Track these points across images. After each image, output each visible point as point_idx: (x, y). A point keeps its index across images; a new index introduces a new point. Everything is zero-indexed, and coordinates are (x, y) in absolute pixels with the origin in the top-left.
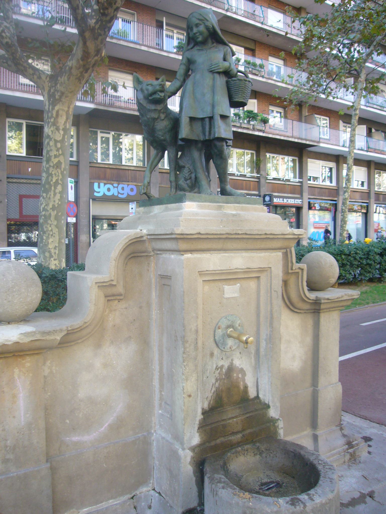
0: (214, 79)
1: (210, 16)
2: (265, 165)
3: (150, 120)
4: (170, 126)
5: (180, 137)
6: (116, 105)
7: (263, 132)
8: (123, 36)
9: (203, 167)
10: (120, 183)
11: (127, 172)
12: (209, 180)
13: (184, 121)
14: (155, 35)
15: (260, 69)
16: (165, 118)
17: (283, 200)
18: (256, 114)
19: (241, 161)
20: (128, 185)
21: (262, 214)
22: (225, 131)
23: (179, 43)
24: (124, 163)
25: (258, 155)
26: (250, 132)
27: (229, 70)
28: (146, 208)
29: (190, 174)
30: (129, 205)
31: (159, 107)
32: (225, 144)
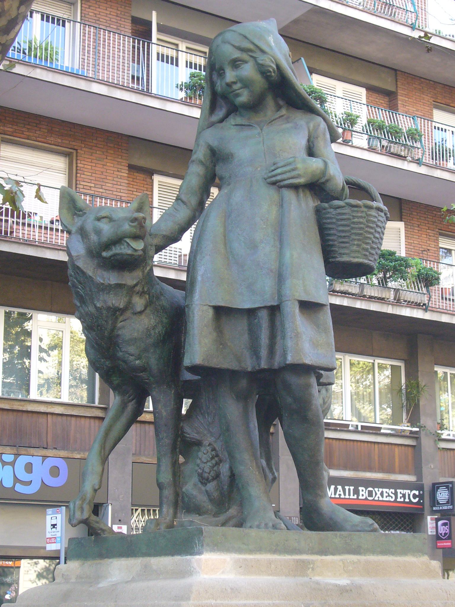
0: (281, 205)
1: (271, 40)
2: (433, 398)
3: (104, 312)
4: (160, 329)
5: (187, 362)
6: (17, 238)
7: (425, 308)
8: (45, 57)
9: (252, 445)
10: (22, 451)
11: (42, 420)
12: (270, 476)
13: (200, 318)
14: (128, 56)
15: (409, 143)
16: (146, 307)
17: (356, 492)
18: (402, 259)
19: (366, 387)
20: (45, 457)
21: (424, 582)
22: (315, 345)
23: (192, 76)
24: (34, 395)
25: (412, 372)
26: (389, 310)
27: (323, 180)
28: (88, 563)
29: (217, 464)
30: (45, 514)
31: (129, 279)
32: (313, 380)
